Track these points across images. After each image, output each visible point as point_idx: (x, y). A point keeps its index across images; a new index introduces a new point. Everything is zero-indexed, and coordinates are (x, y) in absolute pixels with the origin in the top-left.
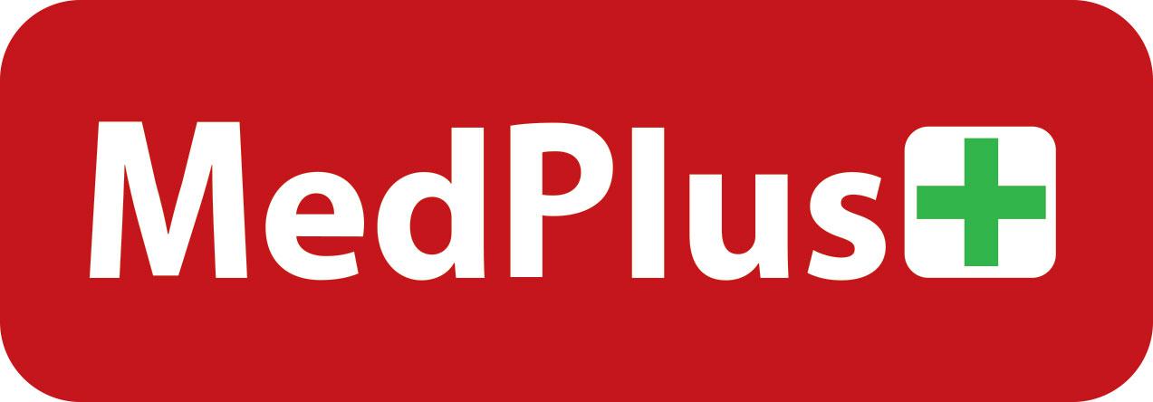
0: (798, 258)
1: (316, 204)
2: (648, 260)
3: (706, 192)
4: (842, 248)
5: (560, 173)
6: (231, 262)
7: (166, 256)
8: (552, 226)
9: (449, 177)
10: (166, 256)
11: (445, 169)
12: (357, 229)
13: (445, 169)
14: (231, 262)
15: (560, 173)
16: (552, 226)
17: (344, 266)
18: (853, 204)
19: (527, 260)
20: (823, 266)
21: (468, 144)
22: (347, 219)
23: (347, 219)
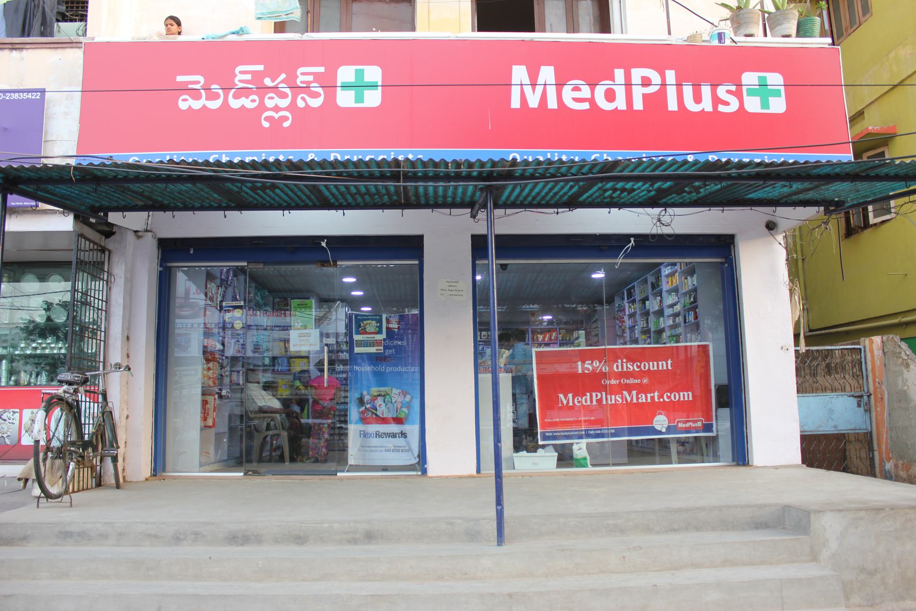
0: (715, 106)
6: (552, 104)
8: (645, 96)
14: (552, 104)
16: (645, 96)
17: (586, 106)
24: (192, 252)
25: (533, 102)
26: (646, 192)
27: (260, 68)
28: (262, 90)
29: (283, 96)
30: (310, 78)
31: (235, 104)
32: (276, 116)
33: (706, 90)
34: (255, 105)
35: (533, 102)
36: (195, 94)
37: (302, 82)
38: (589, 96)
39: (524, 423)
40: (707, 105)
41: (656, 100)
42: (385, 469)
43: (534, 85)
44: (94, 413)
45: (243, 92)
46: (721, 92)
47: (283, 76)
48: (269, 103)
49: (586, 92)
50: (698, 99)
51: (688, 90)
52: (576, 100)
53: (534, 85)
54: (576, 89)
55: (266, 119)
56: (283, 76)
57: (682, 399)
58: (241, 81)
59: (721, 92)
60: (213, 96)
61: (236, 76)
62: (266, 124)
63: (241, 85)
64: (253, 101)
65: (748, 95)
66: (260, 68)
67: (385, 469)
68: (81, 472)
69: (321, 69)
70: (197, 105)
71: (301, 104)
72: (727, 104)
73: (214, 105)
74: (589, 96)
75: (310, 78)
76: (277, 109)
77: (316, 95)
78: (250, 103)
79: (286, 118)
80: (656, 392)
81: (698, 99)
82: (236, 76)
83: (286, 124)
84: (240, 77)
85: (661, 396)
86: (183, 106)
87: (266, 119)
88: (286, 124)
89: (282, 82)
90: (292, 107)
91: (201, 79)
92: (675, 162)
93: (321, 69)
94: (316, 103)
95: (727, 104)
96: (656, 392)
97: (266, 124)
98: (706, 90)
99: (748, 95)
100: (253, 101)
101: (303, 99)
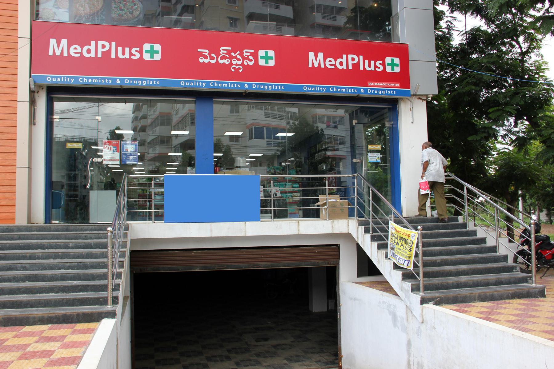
0: (130, 56)
1: (76, 49)
2: (113, 56)
3: (367, 62)
4: (379, 68)
5: (353, 59)
6: (65, 54)
7: (316, 65)
8: (102, 52)
9: (91, 46)
10: (316, 65)
11: (90, 45)
12: (334, 63)
13: (90, 45)
14: (65, 54)
15: (103, 46)
16: (102, 52)
17: (79, 55)
18: (380, 64)
19: (100, 55)
20: (133, 57)
21: (93, 43)
22: (333, 63)
23: (333, 63)
25: (58, 53)
27: (230, 48)
28: (231, 58)
29: (239, 60)
30: (249, 54)
31: (221, 62)
32: (237, 67)
33: (127, 50)
34: (228, 63)
35: (58, 53)
36: (206, 57)
37: (245, 55)
38: (80, 52)
40: (127, 56)
41: (356, 66)
43: (58, 47)
44: (334, 255)
45: (222, 58)
46: (378, 63)
47: (238, 52)
48: (234, 62)
49: (79, 50)
50: (123, 53)
51: (120, 49)
52: (330, 65)
53: (58, 47)
54: (330, 61)
55: (233, 68)
56: (238, 52)
58: (222, 53)
60: (212, 58)
62: (233, 70)
63: (223, 55)
64: (228, 61)
66: (230, 48)
69: (252, 51)
70: (206, 61)
71: (246, 63)
72: (135, 55)
73: (213, 61)
74: (80, 52)
75: (249, 54)
76: (237, 65)
77: (251, 60)
78: (227, 62)
79: (240, 69)
81: (123, 53)
83: (241, 71)
84: (222, 51)
86: (201, 61)
87: (233, 68)
88: (241, 71)
89: (238, 55)
90: (242, 64)
91: (207, 51)
93: (252, 51)
94: (251, 63)
95: (135, 55)
97: (233, 70)
98: (127, 50)
100: (228, 61)
101: (246, 61)
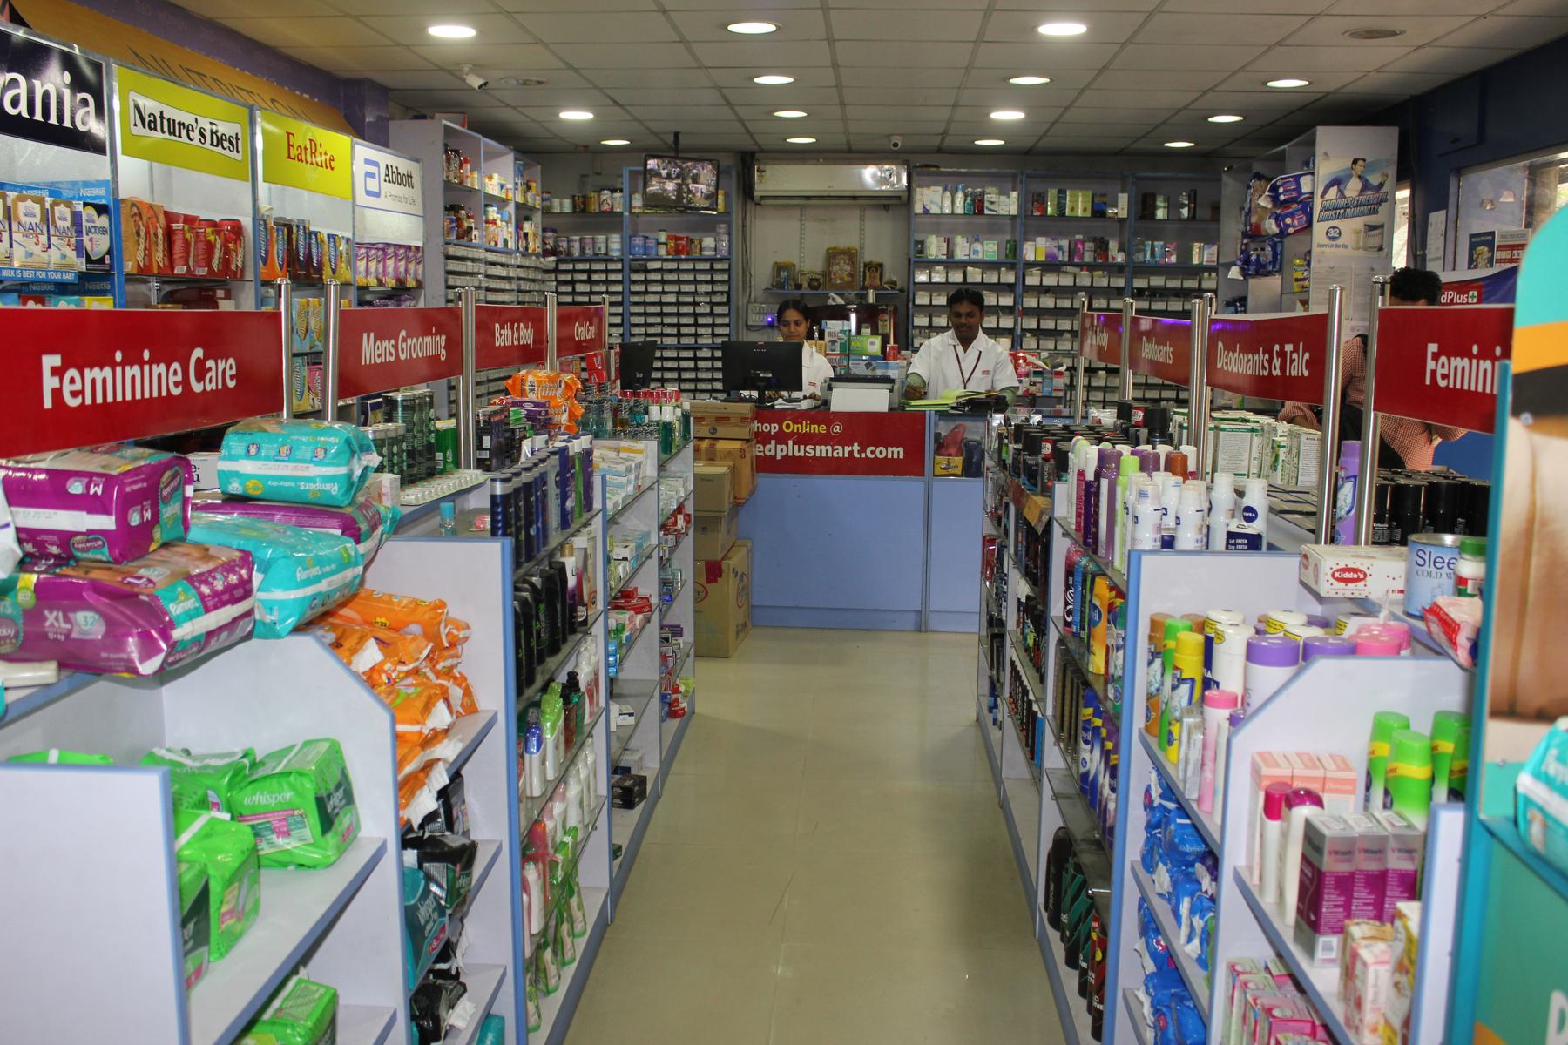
24: (641, 375)
26: (532, 873)
39: (1084, 414)
40: (802, 454)
42: (744, 226)
50: (799, 451)
51: (796, 447)
57: (890, 456)
59: (813, 453)
61: (20, 114)
65: (123, 154)
67: (744, 226)
68: (506, 286)
80: (856, 444)
81: (799, 451)
82: (20, 114)
85: (862, 450)
92: (578, 739)
96: (856, 444)
99: (123, 154)
